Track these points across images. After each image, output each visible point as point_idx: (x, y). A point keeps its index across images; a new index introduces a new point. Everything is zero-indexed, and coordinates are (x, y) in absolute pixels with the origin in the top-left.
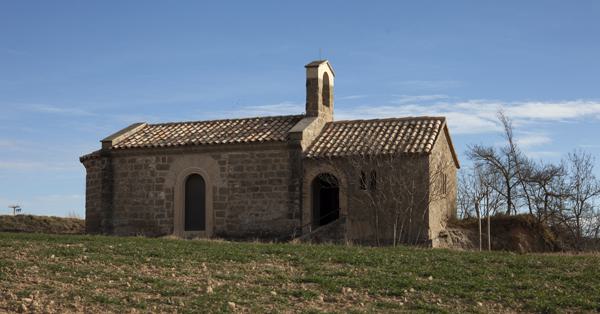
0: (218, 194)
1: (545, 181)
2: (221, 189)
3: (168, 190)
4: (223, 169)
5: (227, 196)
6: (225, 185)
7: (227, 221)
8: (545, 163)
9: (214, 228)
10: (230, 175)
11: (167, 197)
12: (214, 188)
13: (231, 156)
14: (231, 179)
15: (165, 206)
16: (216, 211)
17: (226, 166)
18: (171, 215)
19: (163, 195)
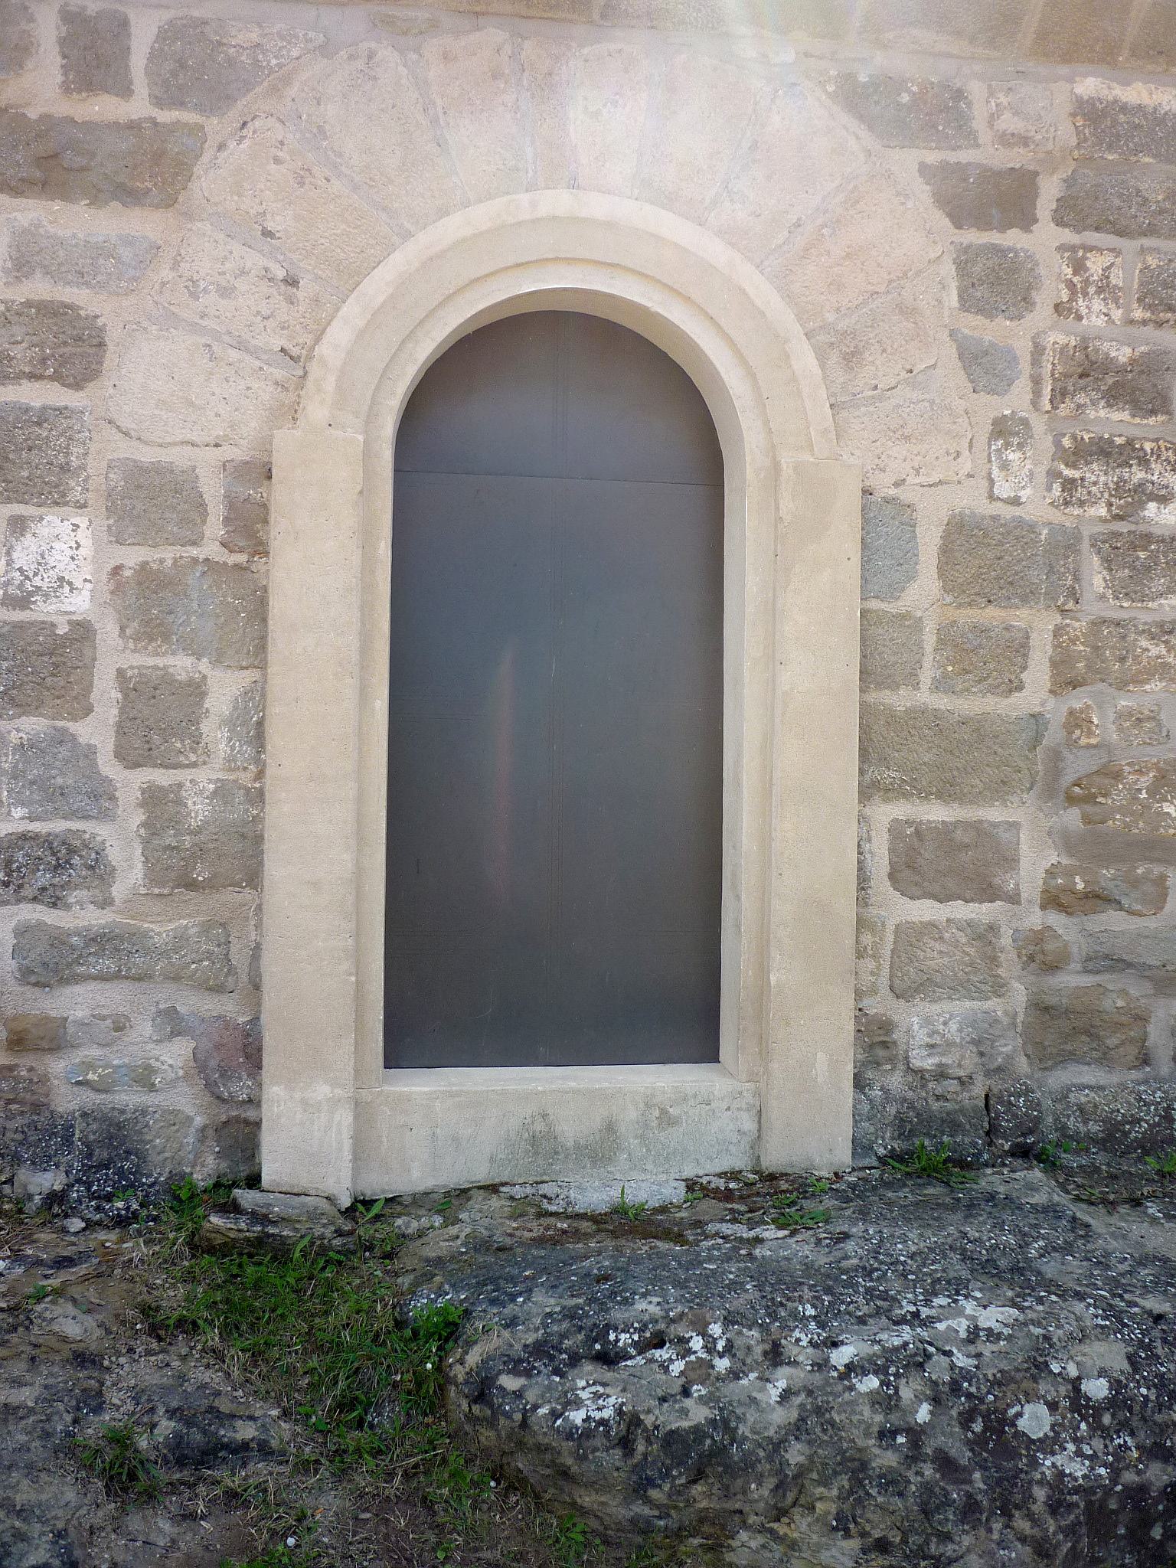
0: (923, 592)
1: (1133, 401)
2: (962, 534)
3: (149, 500)
4: (996, 285)
5: (1040, 625)
6: (1024, 487)
7: (1041, 956)
8: (75, 208)
9: (876, 1042)
10: (1086, 371)
11: (148, 601)
12: (882, 521)
13: (1094, 116)
14: (1113, 421)
15: (96, 731)
16: (886, 813)
17: (1043, 241)
18: (222, 861)
19: (978, 1427)
